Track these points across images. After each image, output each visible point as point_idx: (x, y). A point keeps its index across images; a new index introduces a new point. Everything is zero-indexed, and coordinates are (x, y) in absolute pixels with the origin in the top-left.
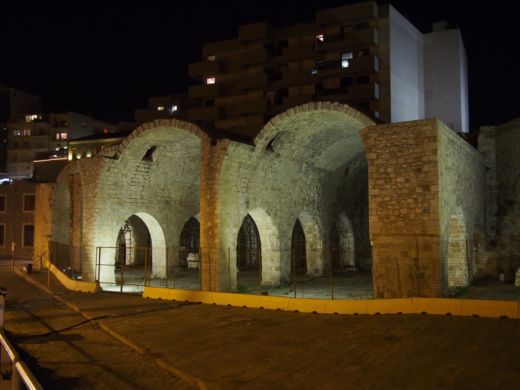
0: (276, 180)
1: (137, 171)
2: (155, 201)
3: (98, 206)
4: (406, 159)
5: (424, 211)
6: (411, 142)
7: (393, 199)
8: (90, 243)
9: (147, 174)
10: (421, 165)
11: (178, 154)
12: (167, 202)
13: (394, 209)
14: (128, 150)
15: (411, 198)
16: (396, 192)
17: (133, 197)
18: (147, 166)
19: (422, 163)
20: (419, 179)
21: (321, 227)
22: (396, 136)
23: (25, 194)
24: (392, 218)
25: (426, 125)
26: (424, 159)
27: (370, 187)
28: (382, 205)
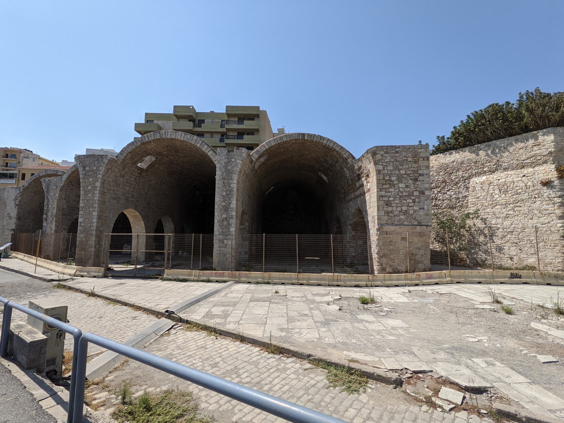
22: (398, 155)
24: (396, 213)
26: (420, 172)
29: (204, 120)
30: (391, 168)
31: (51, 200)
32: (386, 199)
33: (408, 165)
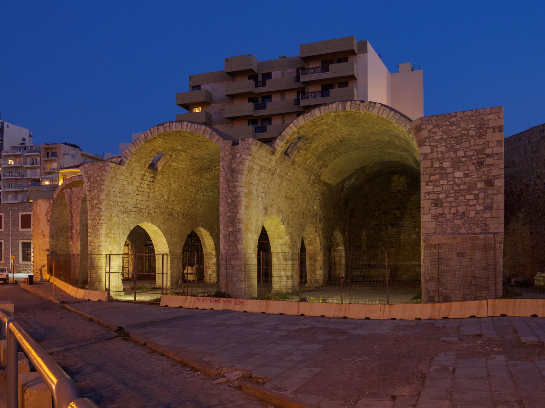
0: (289, 189)
1: (142, 179)
2: (159, 212)
3: (104, 213)
4: (465, 153)
5: (486, 208)
6: (472, 133)
7: (450, 195)
8: (96, 252)
9: (152, 184)
10: (483, 158)
11: (182, 165)
12: (171, 214)
13: (450, 207)
14: (134, 156)
15: (471, 194)
16: (453, 189)
17: (139, 206)
18: (152, 175)
19: (484, 156)
20: (480, 173)
21: (322, 240)
22: (454, 127)
23: (21, 214)
24: (448, 217)
25: (490, 114)
26: (488, 151)
27: (422, 183)
28: (437, 203)
29: (270, 73)
30: (443, 149)
31: (74, 215)
32: (434, 196)
33: (469, 141)
